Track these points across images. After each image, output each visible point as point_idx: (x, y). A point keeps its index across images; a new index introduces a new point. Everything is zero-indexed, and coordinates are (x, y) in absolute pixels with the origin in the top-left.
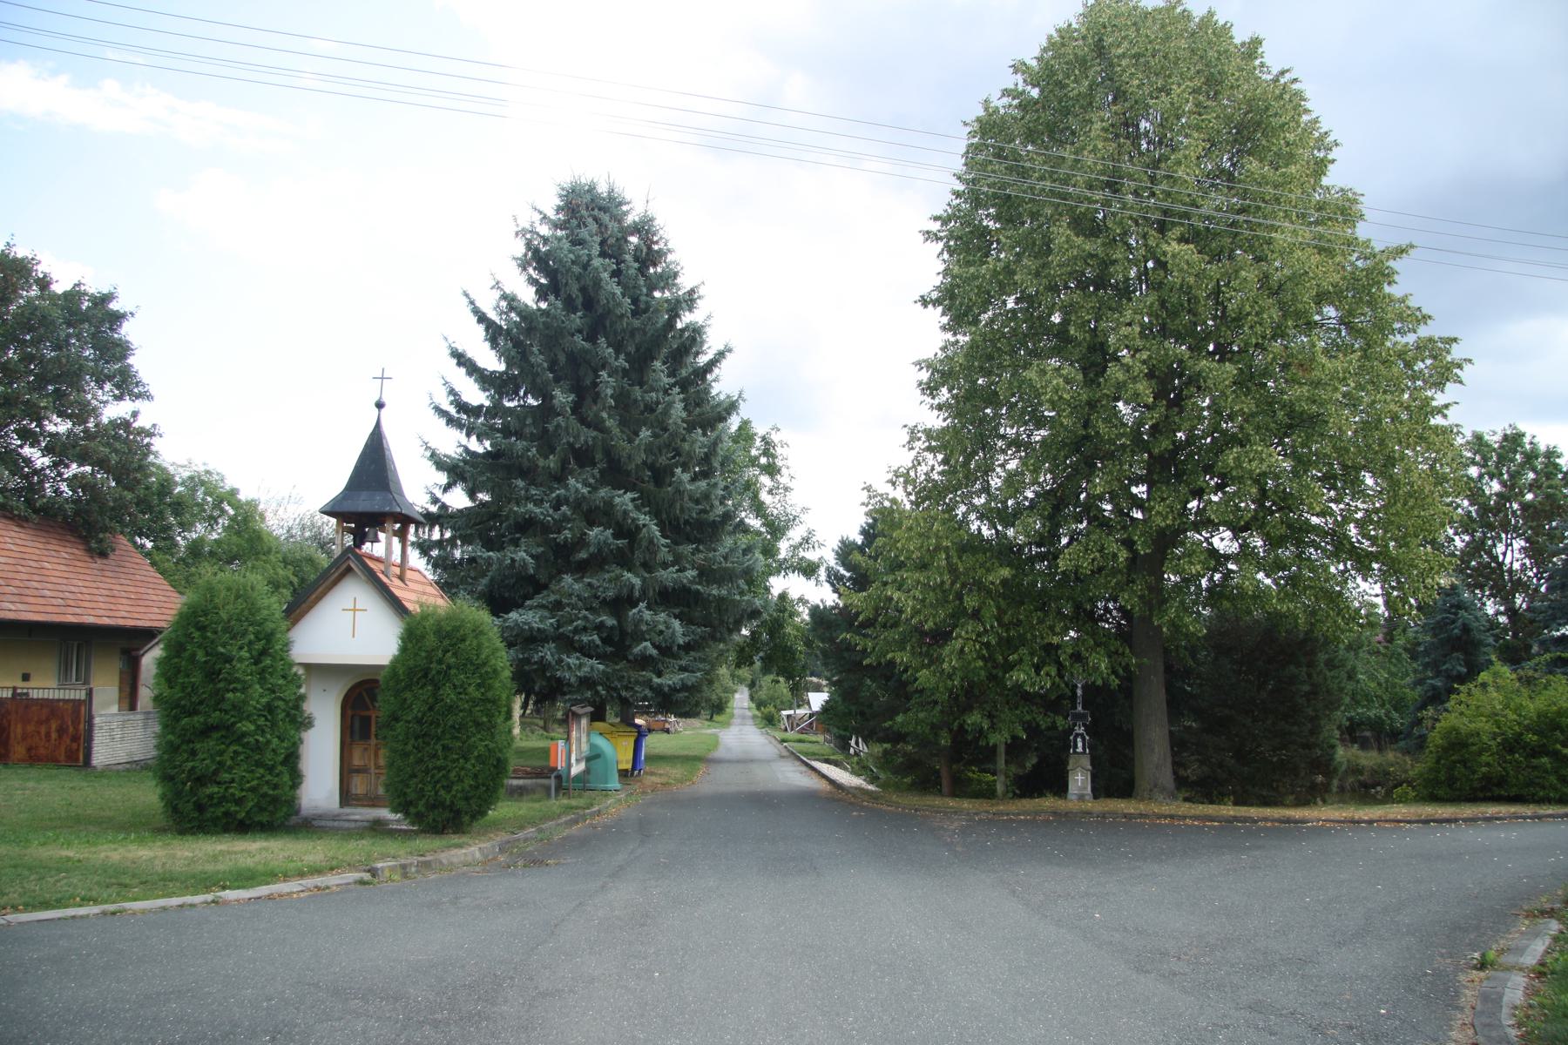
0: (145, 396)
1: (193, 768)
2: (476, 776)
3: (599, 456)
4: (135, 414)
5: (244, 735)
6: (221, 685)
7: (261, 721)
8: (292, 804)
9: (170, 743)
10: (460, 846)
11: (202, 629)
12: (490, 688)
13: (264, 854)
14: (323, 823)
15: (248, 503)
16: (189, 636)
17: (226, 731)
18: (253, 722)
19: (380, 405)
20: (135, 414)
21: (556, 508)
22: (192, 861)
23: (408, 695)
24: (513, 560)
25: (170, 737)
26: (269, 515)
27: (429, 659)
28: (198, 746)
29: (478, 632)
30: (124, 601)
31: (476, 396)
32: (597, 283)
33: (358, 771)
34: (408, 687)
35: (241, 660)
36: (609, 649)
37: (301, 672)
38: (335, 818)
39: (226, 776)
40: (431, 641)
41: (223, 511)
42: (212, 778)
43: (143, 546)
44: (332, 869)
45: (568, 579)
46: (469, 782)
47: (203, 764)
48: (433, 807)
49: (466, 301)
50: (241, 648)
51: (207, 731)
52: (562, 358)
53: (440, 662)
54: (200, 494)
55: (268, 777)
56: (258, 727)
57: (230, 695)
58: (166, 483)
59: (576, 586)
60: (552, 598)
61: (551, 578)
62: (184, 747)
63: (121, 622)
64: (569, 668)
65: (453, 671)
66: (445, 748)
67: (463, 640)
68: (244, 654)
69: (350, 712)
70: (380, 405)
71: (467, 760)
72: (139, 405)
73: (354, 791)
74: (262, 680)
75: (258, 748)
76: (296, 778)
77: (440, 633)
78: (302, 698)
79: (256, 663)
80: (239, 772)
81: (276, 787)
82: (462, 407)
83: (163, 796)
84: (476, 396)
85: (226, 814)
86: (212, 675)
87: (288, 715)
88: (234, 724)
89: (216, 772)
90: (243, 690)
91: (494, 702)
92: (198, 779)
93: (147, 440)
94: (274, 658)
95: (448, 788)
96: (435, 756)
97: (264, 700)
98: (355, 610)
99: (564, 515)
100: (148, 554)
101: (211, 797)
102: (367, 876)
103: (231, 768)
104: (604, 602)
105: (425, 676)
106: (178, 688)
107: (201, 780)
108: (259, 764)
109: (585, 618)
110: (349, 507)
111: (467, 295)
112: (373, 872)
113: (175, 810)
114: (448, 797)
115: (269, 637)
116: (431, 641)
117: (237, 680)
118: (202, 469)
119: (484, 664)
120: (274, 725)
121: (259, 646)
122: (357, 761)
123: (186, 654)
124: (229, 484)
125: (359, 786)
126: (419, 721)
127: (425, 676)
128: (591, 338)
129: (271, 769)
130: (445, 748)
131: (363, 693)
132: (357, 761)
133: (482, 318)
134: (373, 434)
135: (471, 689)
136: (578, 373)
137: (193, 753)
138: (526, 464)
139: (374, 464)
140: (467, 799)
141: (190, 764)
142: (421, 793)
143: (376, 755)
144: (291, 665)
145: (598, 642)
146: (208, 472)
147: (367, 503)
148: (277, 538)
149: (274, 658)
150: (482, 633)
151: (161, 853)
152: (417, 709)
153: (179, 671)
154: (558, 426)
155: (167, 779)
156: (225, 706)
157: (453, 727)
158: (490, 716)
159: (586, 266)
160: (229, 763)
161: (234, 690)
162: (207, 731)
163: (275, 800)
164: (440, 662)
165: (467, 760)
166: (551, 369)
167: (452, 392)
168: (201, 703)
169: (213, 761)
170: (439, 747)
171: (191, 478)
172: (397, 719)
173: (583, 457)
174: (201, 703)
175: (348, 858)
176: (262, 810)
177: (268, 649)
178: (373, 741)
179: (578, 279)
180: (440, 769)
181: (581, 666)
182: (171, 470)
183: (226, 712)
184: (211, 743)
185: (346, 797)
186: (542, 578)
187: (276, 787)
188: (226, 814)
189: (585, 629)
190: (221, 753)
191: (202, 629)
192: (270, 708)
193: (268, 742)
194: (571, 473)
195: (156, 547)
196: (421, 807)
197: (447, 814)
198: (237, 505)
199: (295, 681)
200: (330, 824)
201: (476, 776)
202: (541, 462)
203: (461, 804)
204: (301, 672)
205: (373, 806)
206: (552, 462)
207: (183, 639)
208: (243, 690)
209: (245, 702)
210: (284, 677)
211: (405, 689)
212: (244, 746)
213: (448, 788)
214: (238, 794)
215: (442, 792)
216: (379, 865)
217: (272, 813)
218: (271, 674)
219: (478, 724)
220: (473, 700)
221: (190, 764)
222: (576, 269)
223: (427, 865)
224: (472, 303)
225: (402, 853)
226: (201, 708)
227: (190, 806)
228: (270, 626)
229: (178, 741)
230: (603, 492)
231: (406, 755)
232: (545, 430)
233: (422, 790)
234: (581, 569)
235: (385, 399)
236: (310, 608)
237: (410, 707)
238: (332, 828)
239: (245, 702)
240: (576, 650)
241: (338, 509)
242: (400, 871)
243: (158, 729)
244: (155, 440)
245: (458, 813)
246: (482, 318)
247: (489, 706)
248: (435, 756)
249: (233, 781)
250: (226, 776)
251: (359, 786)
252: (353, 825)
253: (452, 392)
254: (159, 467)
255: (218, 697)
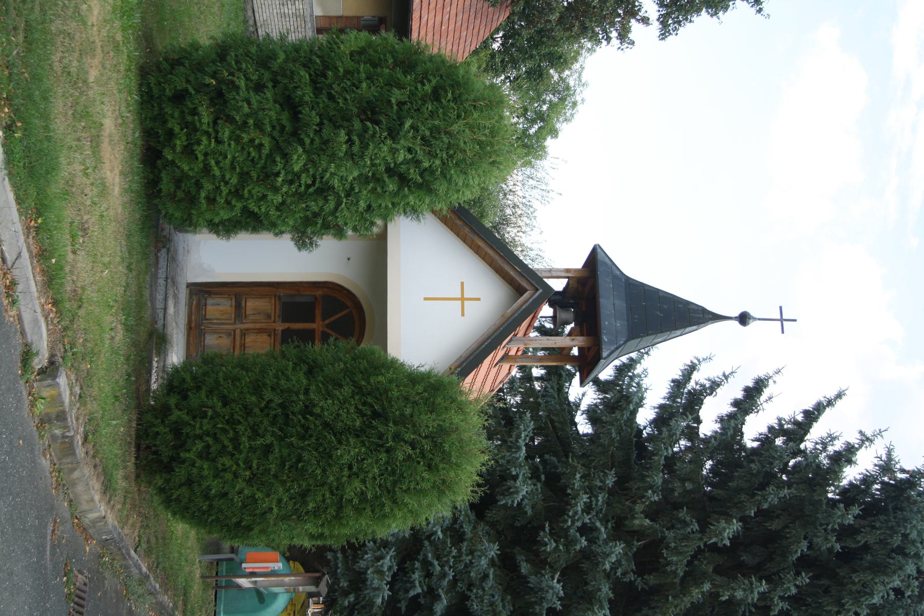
0: (664, 35)
1: (238, 88)
2: (224, 495)
3: (652, 580)
4: (645, 21)
5: (286, 156)
6: (357, 125)
7: (305, 179)
8: (188, 224)
9: (273, 56)
10: (107, 488)
11: (436, 95)
12: (359, 511)
13: (92, 192)
14: (163, 263)
15: (543, 148)
16: (424, 78)
17: (292, 131)
18: (305, 169)
19: (744, 319)
20: (645, 21)
21: (585, 530)
22: (78, 81)
23: (347, 390)
24: (515, 478)
25: (282, 56)
26: (528, 171)
27: (402, 421)
28: (269, 94)
29: (443, 488)
30: (439, 18)
31: (710, 417)
32: (880, 568)
33: (238, 307)
34: (359, 390)
35: (393, 151)
36: (403, 606)
37: (375, 230)
38: (171, 280)
39: (226, 134)
40: (429, 422)
41: (533, 122)
42: (221, 114)
43: (494, 40)
44: (55, 303)
45: (493, 550)
46: (215, 487)
47: (244, 101)
48: (177, 430)
49: (831, 394)
50: (410, 150)
51: (291, 105)
52: (775, 525)
53: (397, 437)
54: (549, 97)
55: (225, 190)
56: (298, 176)
57: (343, 136)
58: (561, 61)
59: (484, 562)
60: (467, 528)
61: (493, 525)
62: (267, 75)
63: (416, 15)
64: (378, 559)
65: (383, 456)
66: (267, 449)
67: (429, 467)
68: (402, 156)
69: (319, 293)
70: (744, 319)
71: (249, 482)
72: (655, 26)
73: (210, 301)
74: (364, 180)
75: (267, 177)
76: (225, 229)
77: (439, 436)
78: (340, 233)
79: (388, 170)
80: (231, 150)
81: (211, 200)
82: (695, 400)
83: (195, 46)
84: (710, 417)
85: (171, 134)
86: (371, 111)
87: (316, 215)
88: (302, 143)
89: (230, 120)
90: (350, 155)
91: (338, 517)
92: (220, 94)
93: (614, 34)
94: (396, 194)
95: (205, 455)
96: (256, 433)
97: (336, 182)
98: (463, 299)
99: (575, 541)
100: (485, 45)
101: (194, 112)
102: (40, 361)
103: (238, 139)
104: (464, 598)
105: (376, 415)
106: (350, 65)
107: (219, 98)
108: (244, 177)
109: (444, 575)
110: (605, 285)
111: (839, 396)
112: (50, 371)
113: (176, 63)
114: (191, 455)
115: (426, 187)
116: (429, 422)
117: (364, 147)
118: (578, 98)
119: (395, 502)
120: (301, 196)
121: (414, 174)
122: (252, 305)
123: (400, 75)
124: (564, 128)
125: (218, 308)
126: (308, 410)
127: (376, 415)
128: (804, 563)
129: (237, 193)
130: (267, 449)
131: (345, 314)
132: (252, 305)
133: (812, 416)
134: (704, 311)
135: (357, 484)
136: (759, 549)
137: (259, 87)
138: (634, 485)
139: (671, 315)
140: (189, 482)
141: (242, 84)
142: (198, 414)
143: (260, 331)
144: (386, 218)
145: (412, 593)
146: (575, 104)
147: (610, 307)
148: (505, 180)
149: (396, 194)
150: (441, 493)
151: (97, 35)
152: (326, 407)
153: (375, 66)
154: (685, 524)
155: (222, 51)
156: (327, 131)
157: (300, 459)
158: (316, 513)
159: (901, 551)
160: (246, 137)
161: (350, 142)
162: (291, 105)
163: (192, 200)
164: (397, 437)
165: (249, 482)
166: (760, 512)
167: (714, 386)
168: (331, 97)
169: (248, 116)
170: (269, 439)
171: (568, 88)
172: (310, 373)
173: (648, 557)
174: (331, 97)
175: (81, 323)
176: (178, 182)
177: (409, 186)
178: (280, 327)
179: (882, 542)
180: (235, 441)
181: (380, 572)
182: (576, 66)
183: (318, 132)
184: (273, 113)
185: (203, 292)
186: (490, 514)
187: (211, 200)
188: (171, 134)
189: (428, 575)
190: (259, 126)
191: (436, 95)
192: (324, 190)
193: (276, 190)
194: (629, 545)
195: (493, 55)
196: (176, 414)
197: (166, 453)
198: (540, 136)
199: (364, 221)
200: (162, 273)
201: (224, 495)
202: (639, 508)
203: (181, 473)
204: (375, 230)
205: (189, 328)
206: (641, 522)
207: (419, 69)
208: (350, 155)
209: (333, 157)
210: (369, 207)
211: (355, 384)
212: (270, 155)
213: (205, 455)
214: (200, 150)
215: (199, 446)
216: (62, 380)
217: (172, 197)
218: (374, 190)
219: (304, 494)
220: (340, 486)
221: (242, 84)
222: (897, 541)
223: (68, 448)
224: (830, 403)
225: (92, 406)
226: (324, 97)
227: (180, 84)
228: (441, 187)
229: (275, 66)
230: (606, 591)
231: (257, 388)
232: (677, 506)
233: (204, 416)
234: (506, 563)
235: (753, 325)
236: (464, 239)
237: (329, 394)
238: (155, 277)
239: (333, 157)
240: (401, 564)
241: (601, 270)
242: (54, 411)
243: (292, 38)
244: (615, 42)
245: (168, 468)
246: (812, 416)
247: (332, 511)
248: (256, 433)
249: (219, 142)
250: (226, 134)
251: (218, 308)
252: (159, 305)
253: (714, 386)
254: (578, 53)
255: (339, 120)
